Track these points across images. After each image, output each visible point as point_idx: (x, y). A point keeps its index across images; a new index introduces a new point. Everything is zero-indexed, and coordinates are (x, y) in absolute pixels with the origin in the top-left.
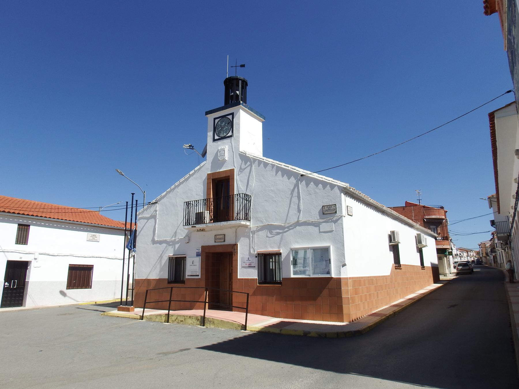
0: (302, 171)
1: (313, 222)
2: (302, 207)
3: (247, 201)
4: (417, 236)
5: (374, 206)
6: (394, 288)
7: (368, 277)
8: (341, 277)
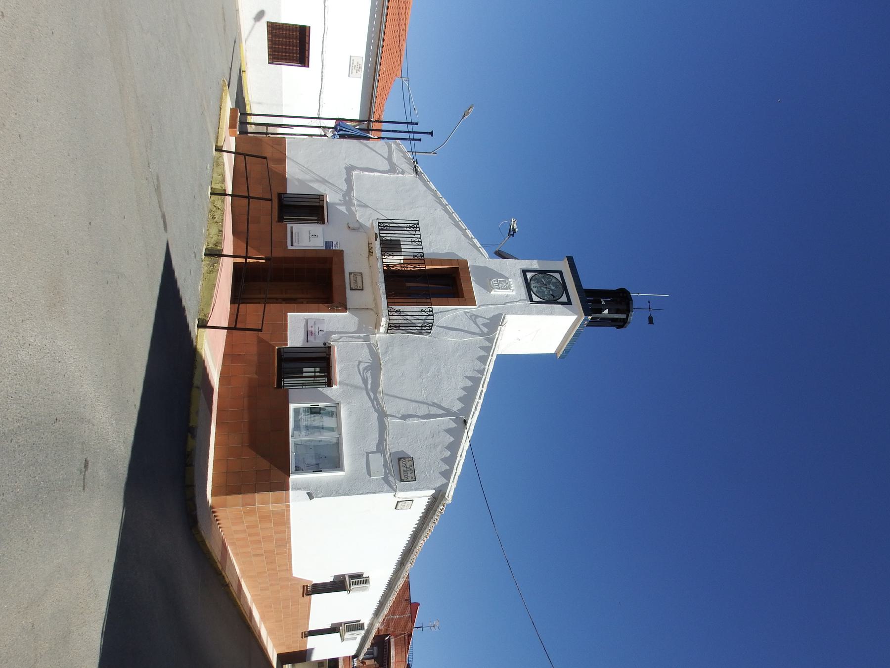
0: (472, 421)
2: (410, 422)
3: (421, 327)
4: (360, 623)
7: (289, 538)
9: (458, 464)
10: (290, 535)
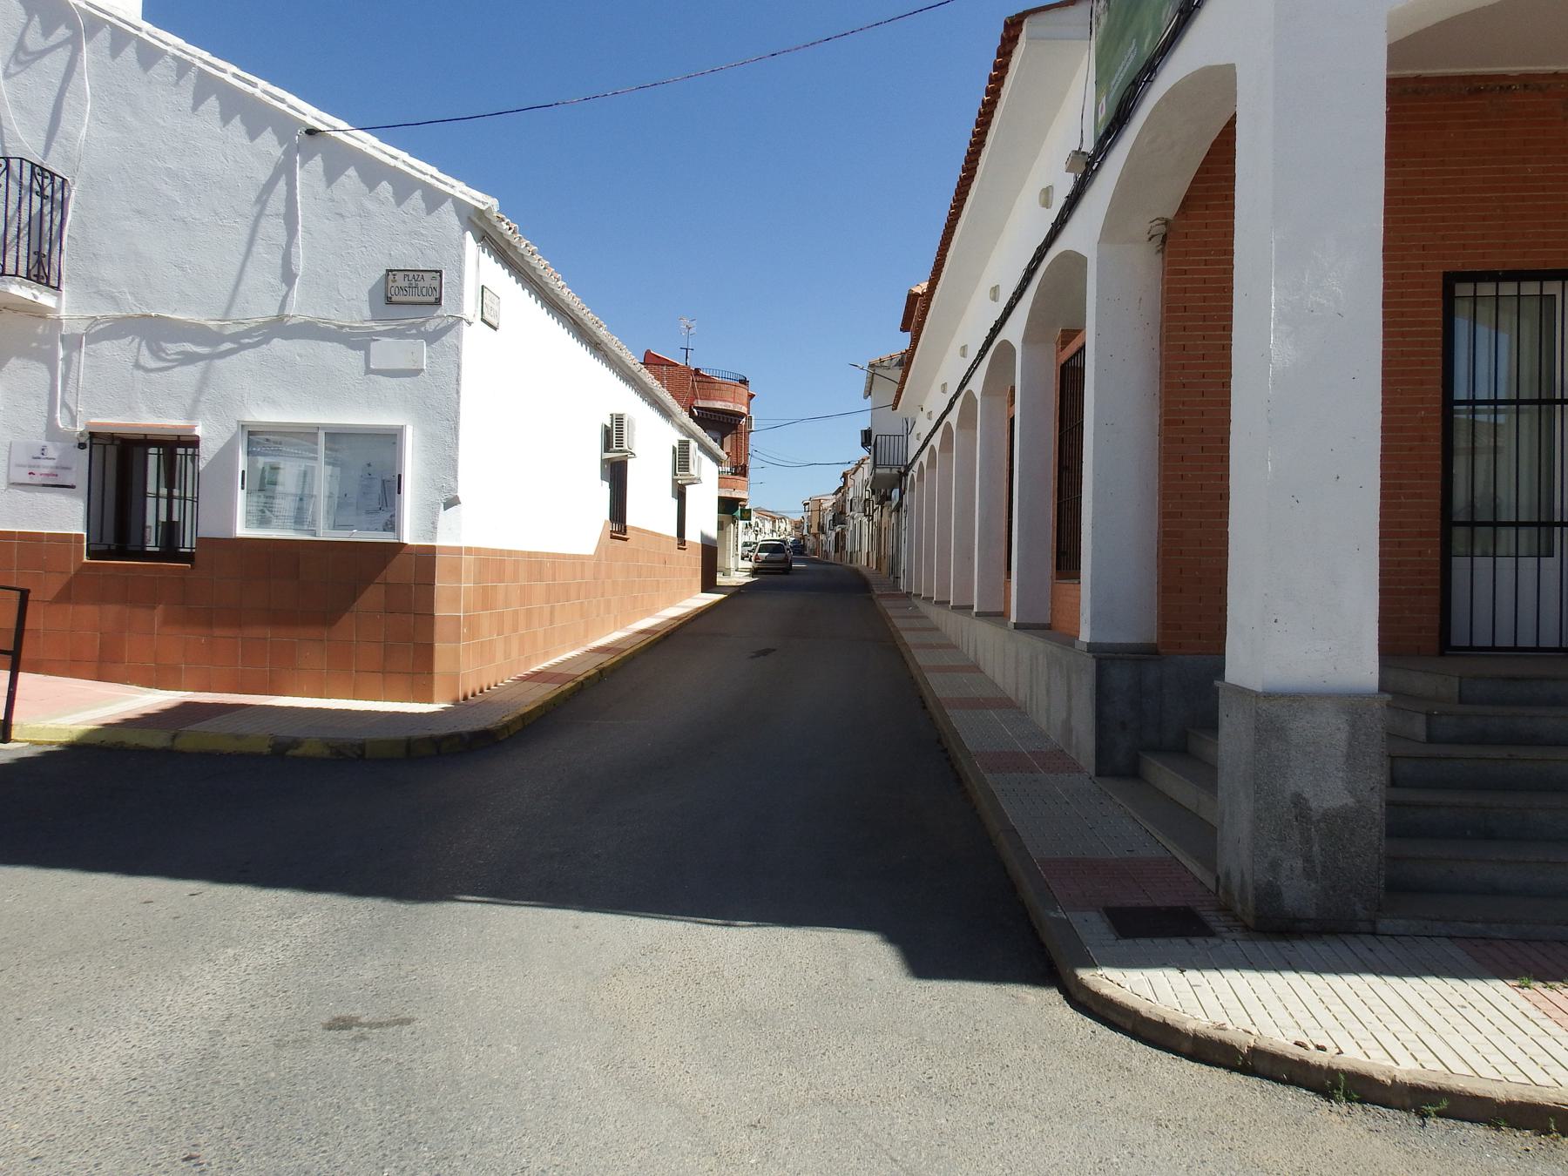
0: (312, 115)
1: (344, 331)
2: (300, 264)
3: (43, 197)
4: (677, 447)
5: (572, 318)
6: (603, 596)
7: (529, 554)
8: (438, 543)
9: (412, 167)
10: (523, 552)
